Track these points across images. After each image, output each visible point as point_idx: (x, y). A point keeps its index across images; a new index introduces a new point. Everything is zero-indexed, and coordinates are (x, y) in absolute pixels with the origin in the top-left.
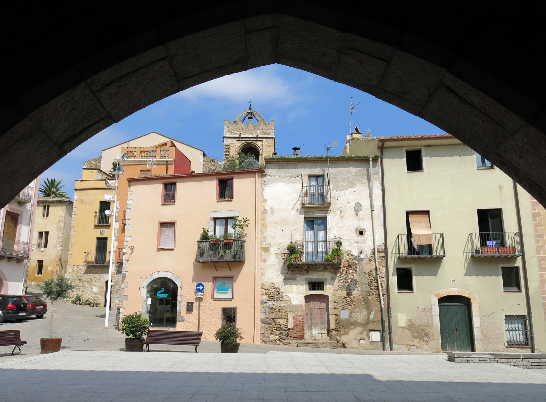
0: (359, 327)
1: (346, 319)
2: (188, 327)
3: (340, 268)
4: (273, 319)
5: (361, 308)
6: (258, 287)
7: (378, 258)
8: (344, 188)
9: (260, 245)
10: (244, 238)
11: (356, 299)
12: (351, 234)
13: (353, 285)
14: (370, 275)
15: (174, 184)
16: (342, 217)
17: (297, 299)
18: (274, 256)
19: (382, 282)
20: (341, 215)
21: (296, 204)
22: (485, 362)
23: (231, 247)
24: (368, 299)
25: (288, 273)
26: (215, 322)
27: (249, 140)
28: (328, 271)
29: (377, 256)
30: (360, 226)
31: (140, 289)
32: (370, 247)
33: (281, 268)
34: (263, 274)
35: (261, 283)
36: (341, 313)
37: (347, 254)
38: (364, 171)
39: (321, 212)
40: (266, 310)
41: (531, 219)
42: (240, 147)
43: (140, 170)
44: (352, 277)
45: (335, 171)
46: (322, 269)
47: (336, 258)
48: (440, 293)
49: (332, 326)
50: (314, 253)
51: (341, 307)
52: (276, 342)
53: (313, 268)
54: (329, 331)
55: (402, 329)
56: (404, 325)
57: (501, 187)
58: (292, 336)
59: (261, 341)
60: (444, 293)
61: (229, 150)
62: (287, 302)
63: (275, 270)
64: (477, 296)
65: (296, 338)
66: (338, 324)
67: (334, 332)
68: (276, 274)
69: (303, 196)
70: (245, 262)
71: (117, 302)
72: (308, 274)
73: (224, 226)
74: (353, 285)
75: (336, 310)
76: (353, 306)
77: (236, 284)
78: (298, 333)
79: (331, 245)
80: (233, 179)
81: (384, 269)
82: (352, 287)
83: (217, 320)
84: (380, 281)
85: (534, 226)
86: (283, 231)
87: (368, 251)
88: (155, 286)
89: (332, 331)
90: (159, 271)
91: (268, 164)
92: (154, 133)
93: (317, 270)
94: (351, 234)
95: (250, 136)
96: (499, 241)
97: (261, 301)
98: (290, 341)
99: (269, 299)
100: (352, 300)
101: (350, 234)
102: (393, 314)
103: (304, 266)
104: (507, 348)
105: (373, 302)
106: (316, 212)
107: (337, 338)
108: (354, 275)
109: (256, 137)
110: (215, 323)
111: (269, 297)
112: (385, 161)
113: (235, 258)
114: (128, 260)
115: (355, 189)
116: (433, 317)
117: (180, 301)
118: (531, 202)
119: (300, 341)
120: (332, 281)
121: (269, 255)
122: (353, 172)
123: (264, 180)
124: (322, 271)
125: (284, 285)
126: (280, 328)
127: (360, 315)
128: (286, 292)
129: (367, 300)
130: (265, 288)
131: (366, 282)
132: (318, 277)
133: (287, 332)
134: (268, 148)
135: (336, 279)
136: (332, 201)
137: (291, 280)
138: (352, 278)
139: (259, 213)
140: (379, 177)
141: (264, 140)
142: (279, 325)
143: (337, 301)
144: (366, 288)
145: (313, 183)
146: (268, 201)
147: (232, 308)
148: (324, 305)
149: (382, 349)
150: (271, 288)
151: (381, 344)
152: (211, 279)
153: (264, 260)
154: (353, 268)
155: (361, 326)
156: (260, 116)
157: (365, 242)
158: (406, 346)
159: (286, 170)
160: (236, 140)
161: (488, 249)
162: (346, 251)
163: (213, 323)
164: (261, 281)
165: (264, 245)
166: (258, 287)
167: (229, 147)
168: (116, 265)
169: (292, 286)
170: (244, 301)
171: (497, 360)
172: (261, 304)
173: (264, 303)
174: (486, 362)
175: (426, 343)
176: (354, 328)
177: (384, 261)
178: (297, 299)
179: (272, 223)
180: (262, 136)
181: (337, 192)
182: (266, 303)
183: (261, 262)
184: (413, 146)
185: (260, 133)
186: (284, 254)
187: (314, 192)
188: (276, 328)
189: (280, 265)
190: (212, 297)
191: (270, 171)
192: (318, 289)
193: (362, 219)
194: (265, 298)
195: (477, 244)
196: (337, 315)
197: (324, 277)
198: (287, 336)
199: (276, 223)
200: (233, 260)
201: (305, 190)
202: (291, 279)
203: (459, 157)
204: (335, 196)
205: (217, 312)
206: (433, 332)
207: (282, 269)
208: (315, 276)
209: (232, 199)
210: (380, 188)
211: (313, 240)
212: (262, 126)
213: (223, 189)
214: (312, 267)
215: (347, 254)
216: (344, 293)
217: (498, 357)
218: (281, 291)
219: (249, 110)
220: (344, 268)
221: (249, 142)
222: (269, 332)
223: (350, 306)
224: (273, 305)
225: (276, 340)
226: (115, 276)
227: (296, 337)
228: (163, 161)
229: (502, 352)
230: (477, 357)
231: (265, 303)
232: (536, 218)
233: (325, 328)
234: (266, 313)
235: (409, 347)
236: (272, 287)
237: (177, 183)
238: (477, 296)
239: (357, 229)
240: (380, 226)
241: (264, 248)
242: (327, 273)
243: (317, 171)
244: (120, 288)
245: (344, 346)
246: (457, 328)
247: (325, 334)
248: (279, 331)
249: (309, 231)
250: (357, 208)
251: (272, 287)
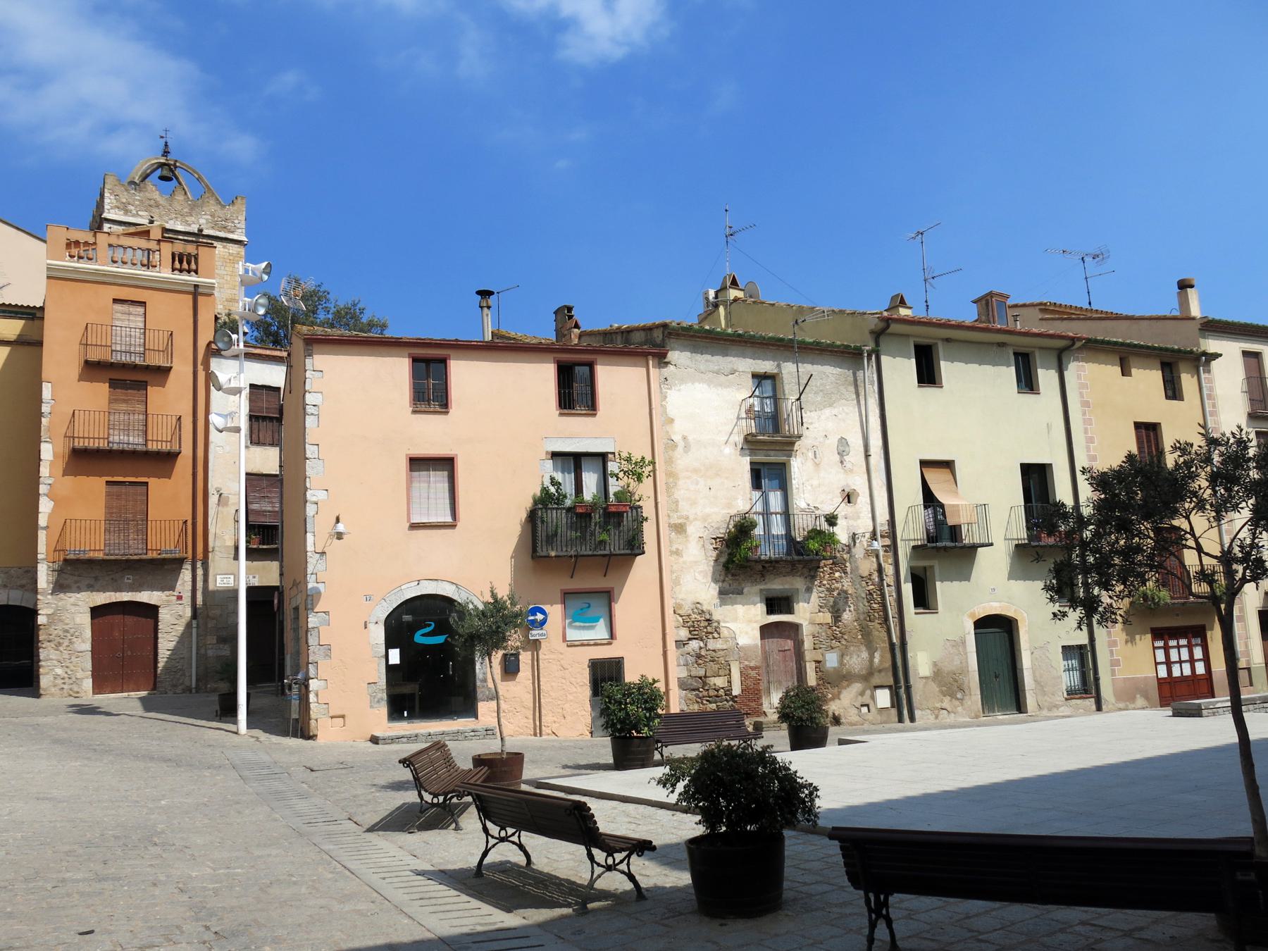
1: (835, 668)
2: (509, 711)
3: (819, 567)
9: (666, 518)
11: (847, 630)
15: (443, 361)
16: (817, 465)
21: (731, 433)
24: (868, 626)
26: (575, 695)
27: (175, 237)
30: (848, 486)
31: (366, 628)
33: (711, 568)
34: (677, 582)
35: (674, 601)
40: (687, 661)
43: (114, 300)
44: (839, 585)
53: (772, 568)
57: (1049, 426)
65: (749, 714)
71: (59, 671)
73: (573, 474)
75: (816, 652)
79: (801, 521)
80: (448, 361)
83: (579, 689)
90: (419, 581)
95: (180, 228)
96: (607, 511)
97: (676, 641)
99: (690, 636)
101: (832, 501)
104: (1066, 699)
110: (574, 697)
111: (690, 632)
114: (323, 553)
115: (836, 409)
116: (968, 654)
118: (1087, 455)
120: (807, 595)
122: (830, 375)
123: (666, 375)
125: (720, 606)
127: (857, 660)
128: (726, 620)
129: (867, 630)
130: (681, 612)
131: (864, 595)
134: (228, 265)
140: (874, 391)
142: (715, 689)
143: (817, 635)
146: (676, 421)
148: (789, 644)
149: (897, 720)
151: (894, 712)
152: (558, 596)
159: (709, 357)
163: (570, 697)
165: (675, 520)
168: (49, 567)
170: (639, 643)
172: (676, 647)
176: (848, 686)
177: (891, 554)
178: (747, 633)
179: (687, 471)
182: (686, 646)
183: (671, 555)
185: (207, 223)
186: (715, 539)
192: (781, 612)
193: (851, 471)
194: (684, 634)
199: (695, 471)
205: (578, 672)
206: (969, 682)
207: (714, 573)
208: (777, 585)
212: (212, 207)
216: (827, 617)
218: (715, 617)
219: (163, 156)
220: (825, 569)
223: (839, 642)
224: (701, 648)
226: (49, 597)
227: (749, 712)
228: (186, 284)
236: (695, 610)
237: (450, 359)
239: (844, 490)
240: (881, 487)
241: (675, 525)
242: (798, 579)
243: (767, 366)
244: (67, 631)
248: (715, 702)
250: (842, 448)
251: (695, 610)
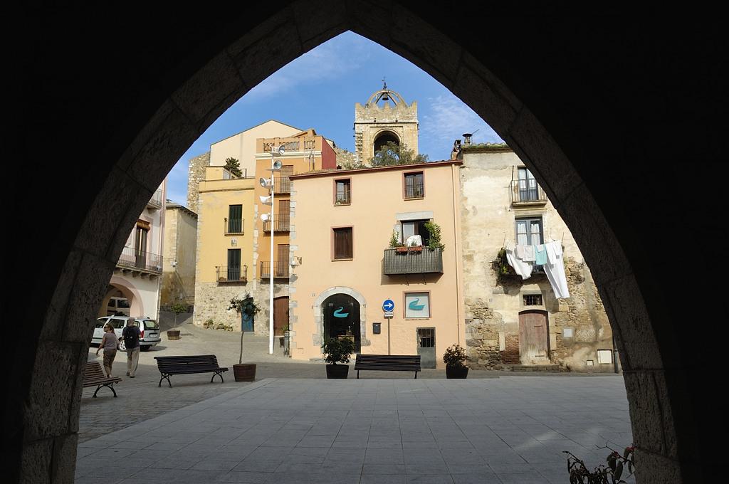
6: (462, 303)
17: (510, 316)
34: (467, 287)
49: (553, 346)
54: (549, 354)
67: (555, 354)
88: (331, 305)
98: (503, 365)
117: (364, 322)
119: (516, 365)
139: (458, 214)
141: (405, 126)
153: (468, 271)
165: (467, 253)
166: (462, 303)
178: (510, 316)
180: (401, 121)
190: (404, 316)
194: (470, 315)
212: (402, 108)
218: (489, 307)
241: (467, 256)
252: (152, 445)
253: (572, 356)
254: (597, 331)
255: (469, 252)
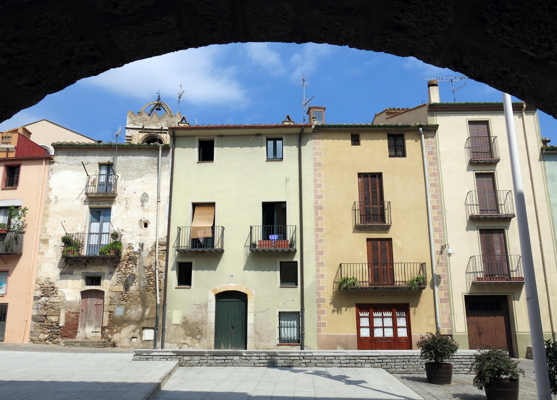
0: (133, 325)
1: (121, 316)
3: (120, 262)
4: (45, 316)
5: (137, 305)
7: (160, 251)
8: (134, 178)
9: (39, 237)
10: (24, 228)
12: (134, 226)
13: (131, 279)
14: (149, 269)
16: (127, 208)
18: (53, 248)
19: (161, 276)
20: (126, 205)
21: (81, 193)
22: (166, 359)
23: (4, 239)
24: (145, 294)
25: (66, 266)
27: (152, 131)
28: (107, 265)
29: (157, 249)
30: (144, 218)
32: (152, 240)
33: (59, 261)
34: (39, 268)
35: (36, 277)
36: (115, 310)
37: (129, 247)
38: (154, 160)
39: (106, 202)
40: (38, 307)
41: (313, 213)
42: (143, 139)
44: (131, 271)
45: (125, 160)
46: (100, 263)
47: (111, 251)
48: (218, 288)
50: (96, 246)
51: (116, 303)
52: (45, 341)
53: (91, 262)
55: (176, 326)
56: (178, 323)
57: (287, 180)
58: (62, 335)
59: (29, 340)
60: (221, 288)
61: (131, 142)
62: (61, 298)
63: (52, 263)
64: (254, 292)
65: (67, 336)
66: (111, 321)
67: (106, 330)
68: (53, 267)
69: (90, 184)
70: (22, 255)
72: (86, 268)
74: (131, 279)
76: (129, 302)
77: (10, 279)
78: (69, 331)
80: (21, 166)
81: (163, 263)
82: (130, 282)
84: (159, 276)
85: (316, 220)
86: (65, 222)
87: (148, 246)
89: (105, 329)
91: (58, 151)
92: (45, 121)
93: (96, 264)
94: (134, 226)
95: (154, 128)
97: (34, 297)
98: (59, 340)
99: (43, 295)
100: (128, 295)
102: (168, 311)
103: (83, 260)
105: (150, 298)
106: (101, 203)
107: (108, 336)
108: (133, 269)
109: (160, 129)
112: (177, 150)
113: (7, 250)
118: (314, 195)
121: (48, 247)
124: (101, 264)
126: (50, 327)
127: (135, 312)
130: (40, 283)
131: (145, 277)
132: (95, 272)
133: (58, 330)
135: (115, 274)
136: (118, 191)
137: (67, 274)
138: (131, 272)
143: (113, 297)
144: (144, 283)
145: (104, 172)
147: (4, 304)
150: (46, 283)
153: (42, 253)
154: (133, 262)
155: (134, 323)
156: (167, 107)
157: (148, 235)
158: (178, 345)
159: (76, 157)
160: (139, 132)
161: (264, 243)
162: (127, 244)
164: (36, 275)
165: (44, 237)
167: (131, 138)
169: (68, 280)
171: (180, 358)
172: (34, 300)
173: (37, 299)
174: (167, 360)
175: (198, 341)
176: (127, 326)
178: (72, 294)
181: (125, 182)
182: (39, 299)
184: (206, 135)
187: (104, 181)
188: (48, 326)
189: (58, 259)
191: (59, 158)
192: (96, 285)
193: (147, 210)
194: (39, 293)
195: (258, 236)
196: (112, 312)
197: (102, 272)
198: (58, 335)
199: (59, 213)
200: (4, 252)
201: (93, 179)
202: (68, 273)
203: (249, 147)
204: (122, 185)
206: (206, 330)
207: (59, 263)
208: (93, 270)
209: (17, 187)
210: (169, 178)
211: (98, 232)
213: (12, 177)
214: (92, 261)
215: (129, 247)
216: (121, 288)
217: (181, 355)
218: (56, 286)
221: (153, 134)
222: (40, 330)
223: (127, 302)
224: (47, 301)
225: (46, 339)
227: (66, 335)
228: (3, 148)
229: (272, 350)
230: (157, 355)
231: (38, 300)
232: (318, 212)
233: (99, 326)
234: (38, 310)
235: (181, 345)
236: (47, 282)
238: (254, 292)
242: (105, 267)
243: (106, 159)
245: (114, 345)
246: (233, 325)
247: (99, 332)
249: (94, 223)
250: (144, 199)
252: (113, 357)
253: (120, 333)
254: (144, 311)
255: (46, 236)
